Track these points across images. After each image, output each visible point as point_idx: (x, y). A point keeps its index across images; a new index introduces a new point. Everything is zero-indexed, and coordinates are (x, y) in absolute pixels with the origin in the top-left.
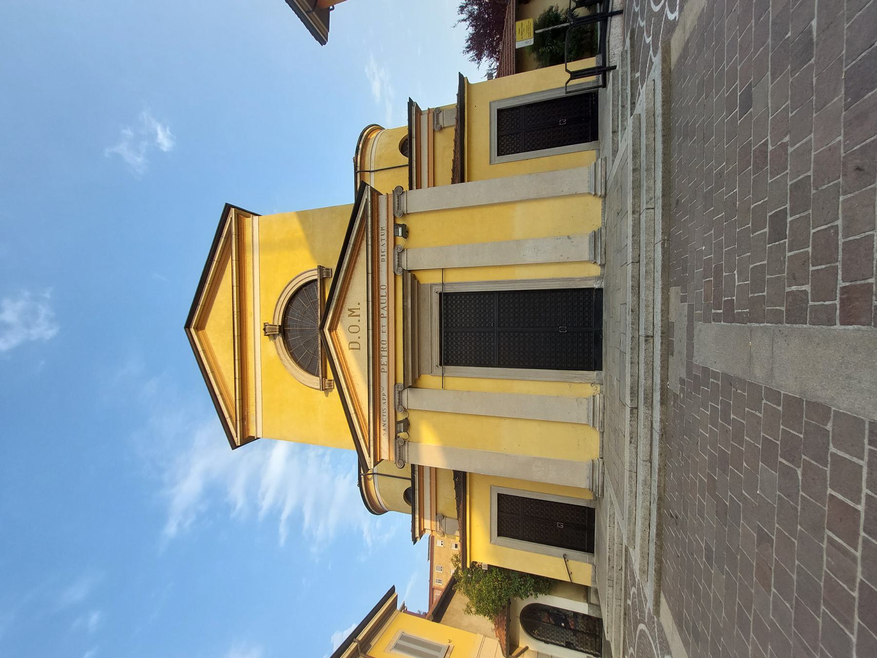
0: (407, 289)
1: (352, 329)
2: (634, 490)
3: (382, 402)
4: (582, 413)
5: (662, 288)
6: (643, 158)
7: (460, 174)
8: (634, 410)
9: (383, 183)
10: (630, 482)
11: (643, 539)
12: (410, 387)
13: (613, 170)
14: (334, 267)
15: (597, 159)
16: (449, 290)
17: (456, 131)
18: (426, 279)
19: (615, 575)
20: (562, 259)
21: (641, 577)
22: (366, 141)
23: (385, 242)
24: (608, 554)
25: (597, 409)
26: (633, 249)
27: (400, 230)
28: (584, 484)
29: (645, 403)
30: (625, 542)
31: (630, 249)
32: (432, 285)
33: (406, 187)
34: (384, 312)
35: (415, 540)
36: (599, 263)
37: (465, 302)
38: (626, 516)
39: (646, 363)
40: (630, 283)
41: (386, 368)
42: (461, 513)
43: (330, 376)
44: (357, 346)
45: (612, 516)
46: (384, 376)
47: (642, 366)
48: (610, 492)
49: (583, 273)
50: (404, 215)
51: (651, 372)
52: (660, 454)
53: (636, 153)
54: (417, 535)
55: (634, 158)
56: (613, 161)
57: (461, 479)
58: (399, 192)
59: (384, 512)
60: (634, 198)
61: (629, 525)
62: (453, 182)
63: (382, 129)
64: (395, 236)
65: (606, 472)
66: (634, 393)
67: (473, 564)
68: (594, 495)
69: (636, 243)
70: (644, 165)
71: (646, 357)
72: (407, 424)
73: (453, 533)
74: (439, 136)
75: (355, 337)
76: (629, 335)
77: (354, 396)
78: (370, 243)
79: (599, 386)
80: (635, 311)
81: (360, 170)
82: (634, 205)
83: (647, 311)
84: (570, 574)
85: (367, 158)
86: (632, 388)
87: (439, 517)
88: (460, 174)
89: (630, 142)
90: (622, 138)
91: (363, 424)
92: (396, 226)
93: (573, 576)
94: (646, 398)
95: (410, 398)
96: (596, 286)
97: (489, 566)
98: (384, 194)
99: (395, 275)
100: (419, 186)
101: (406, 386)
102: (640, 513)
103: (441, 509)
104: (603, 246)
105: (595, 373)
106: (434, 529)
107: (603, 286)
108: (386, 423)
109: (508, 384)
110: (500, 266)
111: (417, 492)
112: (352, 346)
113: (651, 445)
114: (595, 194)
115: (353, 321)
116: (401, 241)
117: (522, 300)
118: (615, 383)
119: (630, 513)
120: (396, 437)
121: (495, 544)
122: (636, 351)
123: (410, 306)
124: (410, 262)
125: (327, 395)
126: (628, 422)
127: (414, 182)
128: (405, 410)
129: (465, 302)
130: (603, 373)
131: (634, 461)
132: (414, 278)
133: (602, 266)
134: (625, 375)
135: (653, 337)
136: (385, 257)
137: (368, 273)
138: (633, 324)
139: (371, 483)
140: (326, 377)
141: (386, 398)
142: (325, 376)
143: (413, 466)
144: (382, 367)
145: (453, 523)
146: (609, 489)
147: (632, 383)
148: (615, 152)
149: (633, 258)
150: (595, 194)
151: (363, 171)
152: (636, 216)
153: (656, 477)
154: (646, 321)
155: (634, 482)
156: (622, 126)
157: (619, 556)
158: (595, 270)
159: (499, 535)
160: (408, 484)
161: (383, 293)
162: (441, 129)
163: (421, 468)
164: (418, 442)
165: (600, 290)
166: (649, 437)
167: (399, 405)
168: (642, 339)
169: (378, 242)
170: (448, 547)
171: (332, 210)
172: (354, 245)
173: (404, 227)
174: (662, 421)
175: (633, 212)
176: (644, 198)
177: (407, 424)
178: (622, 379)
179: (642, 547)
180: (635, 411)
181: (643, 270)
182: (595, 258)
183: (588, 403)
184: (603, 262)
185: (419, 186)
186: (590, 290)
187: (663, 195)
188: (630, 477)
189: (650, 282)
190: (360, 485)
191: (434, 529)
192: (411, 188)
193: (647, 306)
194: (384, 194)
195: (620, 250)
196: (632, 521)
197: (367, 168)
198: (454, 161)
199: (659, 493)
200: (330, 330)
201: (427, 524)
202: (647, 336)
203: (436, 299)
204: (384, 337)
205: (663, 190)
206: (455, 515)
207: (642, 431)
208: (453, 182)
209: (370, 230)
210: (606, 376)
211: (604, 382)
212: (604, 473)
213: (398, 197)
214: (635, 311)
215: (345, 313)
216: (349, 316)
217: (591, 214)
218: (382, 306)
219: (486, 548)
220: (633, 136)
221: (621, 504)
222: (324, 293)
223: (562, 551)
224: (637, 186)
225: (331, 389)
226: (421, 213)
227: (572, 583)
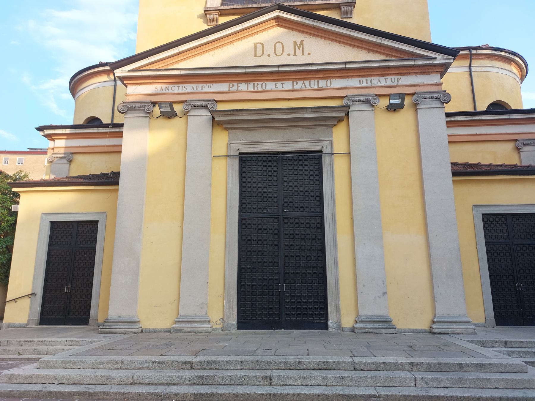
0: (327, 112)
1: (279, 46)
2: (101, 367)
3: (195, 86)
4: (190, 309)
5: (324, 395)
6: (474, 375)
7: (462, 171)
8: (190, 365)
9: (455, 79)
10: (110, 362)
11: (46, 377)
12: (213, 117)
13: (462, 342)
14: (354, 20)
15: (475, 325)
16: (325, 161)
17: (515, 166)
18: (338, 134)
19: (13, 348)
20: (360, 286)
21: (5, 376)
22: (508, 60)
23: (383, 83)
24: (36, 340)
25: (196, 325)
26: (370, 363)
27: (397, 101)
28: (113, 313)
29: (197, 377)
30: (46, 358)
31: (369, 360)
32: (330, 141)
33: (450, 108)
34: (299, 85)
35: (41, 129)
36: (357, 326)
37: (312, 180)
38: (73, 359)
39: (241, 377)
40: (331, 359)
41: (234, 89)
42: (73, 181)
43: (223, 20)
44: (259, 52)
45: (78, 344)
46: (224, 87)
47: (238, 373)
48: (103, 340)
49: (344, 308)
50: (415, 106)
51: (231, 382)
52: (139, 394)
53: (481, 367)
54: (47, 132)
55: (475, 365)
56: (472, 342)
57: (111, 180)
58: (444, 98)
59: (74, 97)
60: (429, 364)
61: (62, 362)
62: (453, 165)
63: (522, 79)
64: (389, 95)
65: (126, 336)
66: (208, 365)
67: (17, 195)
68: (103, 324)
69: (377, 367)
70: (466, 376)
71: (248, 377)
72: (170, 115)
73: (52, 172)
74: (509, 146)
75: (269, 50)
76: (273, 359)
77: (199, 50)
78: (383, 64)
79: (220, 326)
80: (299, 366)
81: (473, 53)
82: (420, 364)
83: (299, 378)
84: (15, 300)
85: (486, 62)
86: (213, 362)
87: (69, 157)
88: (462, 171)
89: (494, 361)
90: (499, 352)
91: (167, 62)
92: (402, 96)
93: (13, 303)
94: (202, 377)
95: (200, 119)
96: (330, 323)
97: (16, 213)
98: (442, 81)
99: (343, 97)
100: (450, 124)
101: (213, 113)
102: (75, 374)
103: (79, 159)
104: (375, 331)
105: (235, 323)
106: (56, 151)
107: (330, 330)
108: (170, 91)
109: (221, 229)
110: (352, 218)
111: (95, 130)
112: (259, 47)
113: (150, 384)
114: (434, 322)
115: (289, 48)
116: (384, 102)
117: (314, 242)
118: (222, 344)
119: (75, 363)
120: (154, 103)
121: (42, 218)
122: (254, 366)
123: (306, 115)
124: (359, 114)
125: (200, 17)
126: (177, 358)
127: (455, 119)
128: (186, 113)
129: (312, 180)
130: (235, 331)
131: (133, 366)
132: (340, 120)
133: (353, 330)
134: (229, 354)
135: (271, 384)
136: (364, 84)
137: (345, 63)
138: (285, 363)
139: (104, 78)
140: (221, 15)
141: (200, 90)
142: (222, 13)
143: (121, 125)
144: (235, 84)
145: (63, 172)
146: (107, 339)
147: (219, 362)
148: (483, 344)
149: (359, 363)
150: (434, 322)
151: (471, 57)
152: (408, 367)
153: (115, 389)
154: (288, 377)
155: (109, 366)
156: (513, 352)
157: (34, 352)
158: (348, 322)
159: (52, 223)
160: (106, 120)
161: (322, 83)
162: (518, 149)
163: (120, 135)
164: (150, 129)
165: (325, 327)
166: (160, 382)
167: (192, 106)
168: (268, 373)
169: (383, 75)
170: (37, 169)
171: (425, 16)
172: (380, 45)
173: (401, 106)
174: (176, 395)
175: (411, 364)
176: (428, 376)
177: (170, 115)
178: (225, 351)
179: (37, 376)
180: (188, 366)
181: (346, 374)
182: (362, 322)
183: (202, 316)
184: (356, 331)
185: (450, 124)
186: (326, 317)
187: (430, 397)
188: (116, 363)
189: (332, 381)
190: (101, 65)
191: (56, 151)
192: (448, 115)
193: (304, 378)
194: (442, 81)
195: (369, 350)
196: (67, 365)
197: (475, 63)
198: (478, 165)
199: (96, 394)
200: (277, 18)
201: (61, 143)
202: (271, 379)
203: (315, 147)
204: (271, 86)
205: (437, 397)
206: (74, 174)
207: (166, 375)
208: (453, 165)
209: (399, 63)
210: (231, 334)
211: (224, 332)
212: (125, 333)
213: (437, 98)
214: (299, 366)
215: (298, 37)
216: (295, 43)
217: (412, 317)
218: (307, 82)
219: (35, 211)
220: (502, 365)
221: (88, 353)
222: (323, 9)
223: (40, 291)
224: (442, 368)
225: (207, 21)
226: (417, 126)
227: (5, 302)
